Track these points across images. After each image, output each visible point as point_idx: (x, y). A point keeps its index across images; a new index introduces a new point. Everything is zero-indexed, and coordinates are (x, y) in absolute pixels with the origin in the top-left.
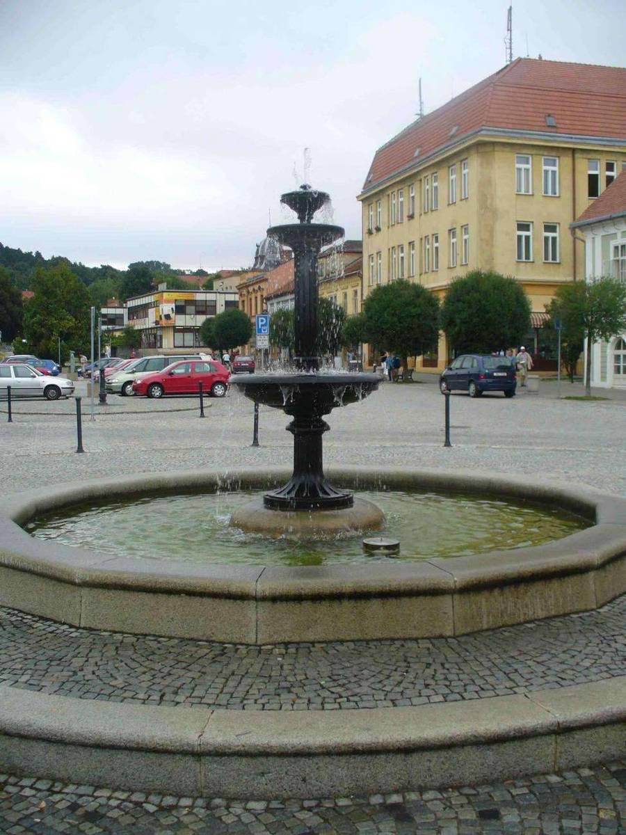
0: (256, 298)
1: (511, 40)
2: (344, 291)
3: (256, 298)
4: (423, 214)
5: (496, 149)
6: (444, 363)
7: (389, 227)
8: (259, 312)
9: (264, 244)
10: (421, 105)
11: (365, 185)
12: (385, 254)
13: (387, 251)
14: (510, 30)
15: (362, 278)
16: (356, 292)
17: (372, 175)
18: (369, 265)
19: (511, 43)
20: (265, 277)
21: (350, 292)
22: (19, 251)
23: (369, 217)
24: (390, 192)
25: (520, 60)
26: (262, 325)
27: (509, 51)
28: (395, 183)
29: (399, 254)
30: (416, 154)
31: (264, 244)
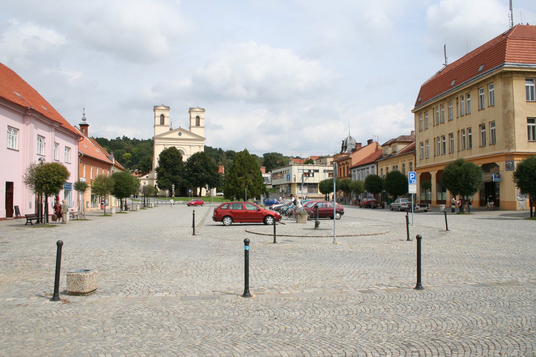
0: (344, 168)
1: (512, 15)
2: (403, 163)
3: (344, 168)
4: (460, 117)
5: (514, 75)
6: (478, 203)
7: (434, 126)
8: (346, 175)
9: (347, 140)
10: (446, 59)
11: (416, 104)
12: (431, 142)
13: (433, 140)
14: (511, 9)
15: (415, 155)
16: (411, 163)
17: (420, 98)
18: (420, 148)
19: (512, 17)
20: (350, 157)
21: (407, 163)
22: (211, 148)
23: (420, 122)
24: (434, 106)
25: (519, 27)
26: (412, 178)
27: (511, 21)
28: (439, 101)
29: (442, 141)
30: (453, 84)
31: (347, 140)
